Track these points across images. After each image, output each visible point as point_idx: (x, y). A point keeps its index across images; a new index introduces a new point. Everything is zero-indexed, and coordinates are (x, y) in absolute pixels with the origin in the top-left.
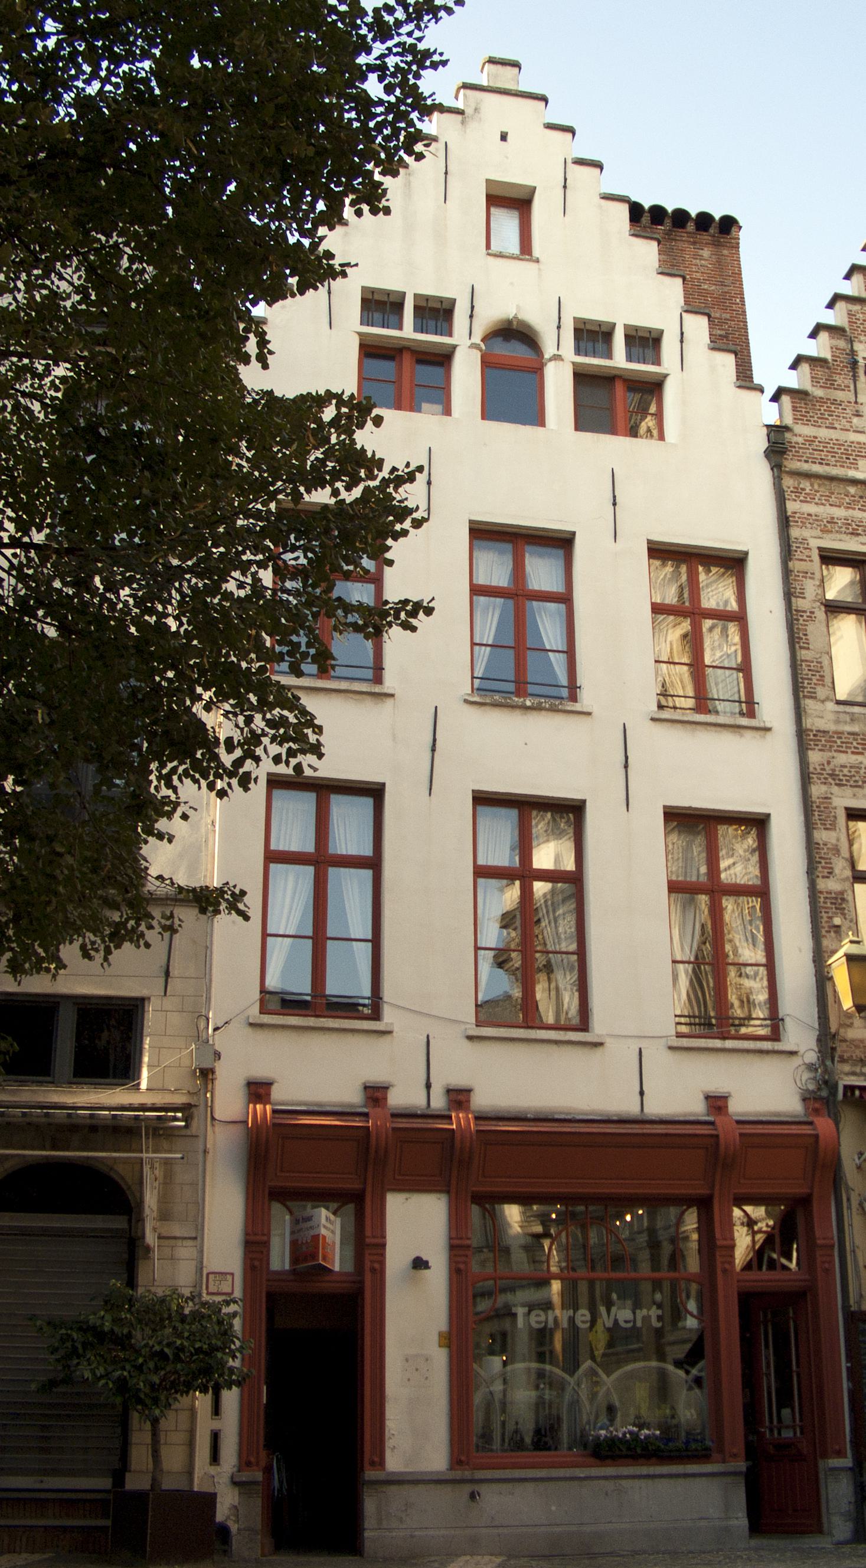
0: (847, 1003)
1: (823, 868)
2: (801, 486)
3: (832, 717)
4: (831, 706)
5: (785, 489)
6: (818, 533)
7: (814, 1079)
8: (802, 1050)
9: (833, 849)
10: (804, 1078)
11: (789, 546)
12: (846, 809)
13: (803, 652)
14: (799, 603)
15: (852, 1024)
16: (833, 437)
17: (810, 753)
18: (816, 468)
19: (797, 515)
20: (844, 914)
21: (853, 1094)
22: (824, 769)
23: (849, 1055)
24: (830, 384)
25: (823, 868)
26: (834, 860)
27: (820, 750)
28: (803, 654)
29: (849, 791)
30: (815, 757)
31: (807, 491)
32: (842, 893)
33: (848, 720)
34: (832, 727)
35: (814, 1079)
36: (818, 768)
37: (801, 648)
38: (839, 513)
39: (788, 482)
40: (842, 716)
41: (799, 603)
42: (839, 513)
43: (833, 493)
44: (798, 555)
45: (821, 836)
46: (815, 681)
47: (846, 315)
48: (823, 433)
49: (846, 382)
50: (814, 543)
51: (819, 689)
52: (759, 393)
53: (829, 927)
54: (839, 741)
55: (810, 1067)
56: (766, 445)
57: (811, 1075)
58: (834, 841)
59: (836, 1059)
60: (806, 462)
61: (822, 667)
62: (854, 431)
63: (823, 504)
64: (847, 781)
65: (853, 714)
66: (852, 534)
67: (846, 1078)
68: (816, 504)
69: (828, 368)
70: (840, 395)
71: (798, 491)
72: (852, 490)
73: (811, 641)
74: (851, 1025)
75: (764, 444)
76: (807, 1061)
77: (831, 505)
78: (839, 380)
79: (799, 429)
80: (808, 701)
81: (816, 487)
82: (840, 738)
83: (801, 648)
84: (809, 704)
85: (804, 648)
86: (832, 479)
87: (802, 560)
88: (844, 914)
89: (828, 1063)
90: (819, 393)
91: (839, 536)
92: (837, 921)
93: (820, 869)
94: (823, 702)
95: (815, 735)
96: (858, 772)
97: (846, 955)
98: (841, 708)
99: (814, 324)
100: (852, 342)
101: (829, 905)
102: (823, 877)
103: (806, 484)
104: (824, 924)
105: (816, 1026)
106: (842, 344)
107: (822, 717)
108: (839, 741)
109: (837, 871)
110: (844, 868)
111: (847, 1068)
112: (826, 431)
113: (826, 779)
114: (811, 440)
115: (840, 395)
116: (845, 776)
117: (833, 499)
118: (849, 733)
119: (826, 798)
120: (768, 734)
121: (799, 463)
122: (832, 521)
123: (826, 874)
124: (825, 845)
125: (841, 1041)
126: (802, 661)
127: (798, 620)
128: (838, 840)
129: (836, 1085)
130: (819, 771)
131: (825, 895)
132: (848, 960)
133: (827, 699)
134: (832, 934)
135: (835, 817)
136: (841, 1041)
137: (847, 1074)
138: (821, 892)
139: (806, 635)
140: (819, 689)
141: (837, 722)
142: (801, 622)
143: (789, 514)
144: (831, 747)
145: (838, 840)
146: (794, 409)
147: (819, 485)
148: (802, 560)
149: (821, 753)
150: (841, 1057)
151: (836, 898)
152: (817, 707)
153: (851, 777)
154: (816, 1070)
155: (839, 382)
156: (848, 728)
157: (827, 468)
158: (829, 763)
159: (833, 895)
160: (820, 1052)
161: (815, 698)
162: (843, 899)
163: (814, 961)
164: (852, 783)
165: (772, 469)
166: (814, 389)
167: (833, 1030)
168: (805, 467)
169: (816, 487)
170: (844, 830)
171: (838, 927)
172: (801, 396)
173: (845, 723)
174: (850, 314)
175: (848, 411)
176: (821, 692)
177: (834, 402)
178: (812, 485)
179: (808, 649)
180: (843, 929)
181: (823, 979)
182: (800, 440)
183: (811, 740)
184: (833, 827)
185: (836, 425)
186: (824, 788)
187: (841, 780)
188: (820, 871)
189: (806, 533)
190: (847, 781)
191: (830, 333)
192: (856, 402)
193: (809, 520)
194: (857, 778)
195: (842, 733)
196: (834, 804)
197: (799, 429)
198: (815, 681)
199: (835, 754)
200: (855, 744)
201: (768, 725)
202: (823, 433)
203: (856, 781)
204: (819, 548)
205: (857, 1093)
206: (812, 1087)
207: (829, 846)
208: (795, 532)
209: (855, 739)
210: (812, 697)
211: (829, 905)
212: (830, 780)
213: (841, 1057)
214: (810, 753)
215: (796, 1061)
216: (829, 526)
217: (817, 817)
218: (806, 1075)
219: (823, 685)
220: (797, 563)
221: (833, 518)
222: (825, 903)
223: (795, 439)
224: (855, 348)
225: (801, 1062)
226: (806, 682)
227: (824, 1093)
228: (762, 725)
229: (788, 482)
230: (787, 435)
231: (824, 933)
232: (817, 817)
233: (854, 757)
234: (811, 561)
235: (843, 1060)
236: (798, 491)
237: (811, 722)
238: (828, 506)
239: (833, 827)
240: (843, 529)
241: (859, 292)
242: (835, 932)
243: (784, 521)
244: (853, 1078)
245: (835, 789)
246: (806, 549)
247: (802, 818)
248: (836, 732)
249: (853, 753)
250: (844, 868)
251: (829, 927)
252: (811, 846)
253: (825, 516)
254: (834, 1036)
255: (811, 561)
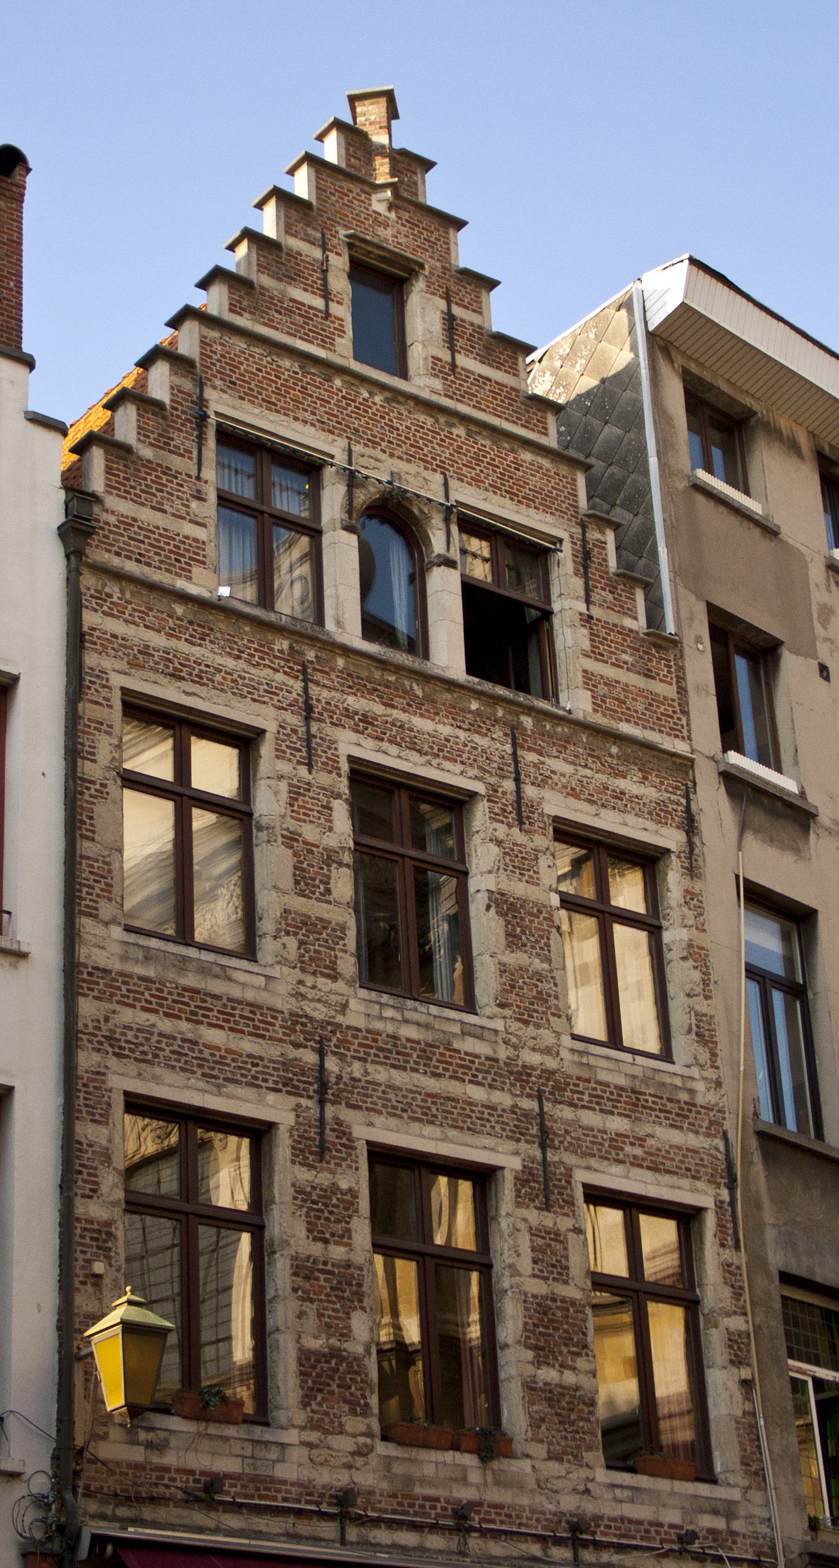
0: (114, 1399)
1: (85, 1181)
2: (107, 590)
3: (117, 949)
4: (117, 932)
5: (83, 590)
6: (122, 665)
7: (44, 1520)
8: (29, 1471)
9: (102, 1154)
10: (28, 1519)
11: (81, 679)
12: (126, 1093)
13: (86, 844)
14: (89, 769)
15: (106, 1434)
16: (161, 524)
17: (81, 1000)
18: (131, 567)
19: (97, 633)
20: (108, 1258)
21: (103, 1549)
22: (99, 1029)
23: (98, 1484)
24: (163, 443)
25: (85, 1181)
26: (102, 1171)
27: (95, 998)
28: (86, 847)
29: (132, 1068)
30: (88, 1008)
31: (115, 599)
32: (108, 1224)
33: (140, 957)
34: (117, 966)
35: (44, 1520)
36: (90, 1024)
37: (83, 836)
38: (158, 640)
39: (89, 581)
40: (132, 950)
41: (89, 769)
42: (158, 640)
43: (151, 610)
44: (91, 695)
45: (87, 1131)
46: (97, 891)
47: (198, 341)
48: (147, 516)
49: (187, 443)
50: (117, 681)
51: (102, 904)
52: (60, 437)
53: (86, 1276)
54: (124, 988)
55: (40, 1501)
56: (63, 519)
57: (40, 1514)
58: (104, 1142)
59: (80, 1490)
60: (118, 554)
61: (110, 871)
62: (191, 521)
63: (134, 623)
64: (132, 1051)
65: (148, 948)
66: (172, 675)
67: (91, 1523)
68: (126, 621)
69: (164, 418)
70: (176, 462)
71: (101, 597)
72: (179, 610)
73: (98, 827)
74: (104, 1437)
75: (58, 517)
76: (35, 1491)
77: (146, 627)
78: (178, 439)
79: (112, 502)
80: (85, 921)
81: (128, 596)
82: (126, 983)
83: (83, 836)
84: (86, 924)
85: (87, 838)
86: (153, 587)
87: (96, 703)
88: (108, 1258)
89: (68, 1496)
90: (146, 452)
91: (153, 676)
92: (99, 1267)
93: (80, 1183)
94: (106, 924)
95: (90, 974)
96: (148, 1039)
97: (123, 1322)
98: (132, 938)
99: (151, 346)
100: (201, 386)
101: (87, 1241)
102: (84, 1196)
103: (113, 589)
104: (78, 1271)
105: (54, 1435)
106: (187, 385)
107: (103, 948)
108: (124, 988)
109: (104, 1189)
110: (116, 1185)
111: (93, 1506)
112: (151, 512)
113: (100, 1043)
114: (128, 523)
115: (176, 462)
116: (128, 1042)
117: (150, 619)
118: (140, 978)
119: (98, 1073)
120: (23, 965)
121: (106, 555)
122: (146, 651)
123: (87, 1192)
124: (90, 1145)
125: (89, 1461)
126: (82, 857)
127: (82, 793)
128: (110, 1141)
129: (78, 1536)
130: (91, 1030)
131: (84, 1225)
132: (124, 1331)
133: (113, 921)
134: (89, 1287)
135: (109, 1105)
136: (89, 1461)
137: (93, 1517)
138: (78, 1220)
139: (91, 818)
140: (102, 904)
141: (125, 958)
142: (86, 797)
143: (85, 629)
144: (112, 995)
145: (110, 1141)
146: (108, 470)
147: (133, 594)
148: (96, 703)
149: (97, 1003)
150: (87, 1487)
151: (99, 1232)
152: (97, 932)
153: (137, 1045)
154: (48, 1506)
155: (177, 442)
156: (139, 970)
157: (146, 569)
158: (107, 1019)
159: (96, 1226)
160: (55, 1476)
161: (96, 916)
162: (109, 1234)
163: (59, 1328)
164: (137, 1055)
165: (67, 557)
166: (140, 446)
167: (79, 1442)
168: (116, 562)
169: (128, 596)
170: (119, 1127)
171: (99, 1276)
172: (123, 453)
173: (137, 961)
174: (204, 343)
175: (185, 489)
176: (106, 910)
177: (167, 471)
178: (122, 591)
179: (93, 840)
180: (107, 1281)
181: (72, 1359)
182: (112, 519)
183: (84, 981)
184: (104, 1119)
185: (166, 507)
186: (96, 1057)
187: (121, 1048)
188: (81, 1187)
189: (107, 663)
190: (132, 1051)
191: (172, 365)
192: (198, 478)
193: (114, 643)
194: (146, 1048)
195: (131, 976)
196: (110, 1084)
197: (112, 502)
198: (97, 891)
199: (118, 1008)
200: (147, 996)
201: (24, 948)
202: (147, 516)
203: (143, 1053)
204: (122, 689)
205: (110, 1549)
206: (38, 1535)
207: (96, 1148)
208: (91, 659)
209: (148, 989)
210: (90, 915)
211: (87, 1241)
212: (106, 1046)
213: (87, 1487)
214: (81, 1000)
215: (19, 1490)
216: (140, 658)
217: (82, 1102)
218: (32, 1515)
219: (110, 899)
220: (89, 705)
221: (147, 647)
222: (82, 1237)
223: (104, 517)
224: (206, 395)
225: (25, 1493)
226: (85, 890)
227: (56, 1546)
228: (15, 947)
229: (89, 581)
230: (96, 509)
231: (77, 1285)
232: (82, 1102)
233: (145, 1016)
234: (110, 707)
235: (89, 1494)
236: (101, 597)
237: (90, 954)
238: (142, 628)
239: (104, 1119)
240: (161, 667)
241: (220, 311)
242: (94, 1285)
243: (77, 639)
244: (102, 1523)
245: (113, 1062)
246: (104, 686)
247: (61, 1100)
248: (121, 974)
249: (143, 1009)
250: (116, 1185)
251: (86, 1276)
252: (70, 1147)
253: (136, 641)
254: (81, 1452)
255: (110, 707)
